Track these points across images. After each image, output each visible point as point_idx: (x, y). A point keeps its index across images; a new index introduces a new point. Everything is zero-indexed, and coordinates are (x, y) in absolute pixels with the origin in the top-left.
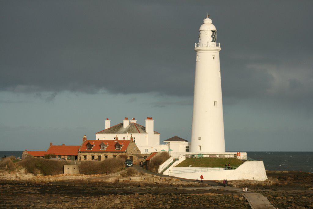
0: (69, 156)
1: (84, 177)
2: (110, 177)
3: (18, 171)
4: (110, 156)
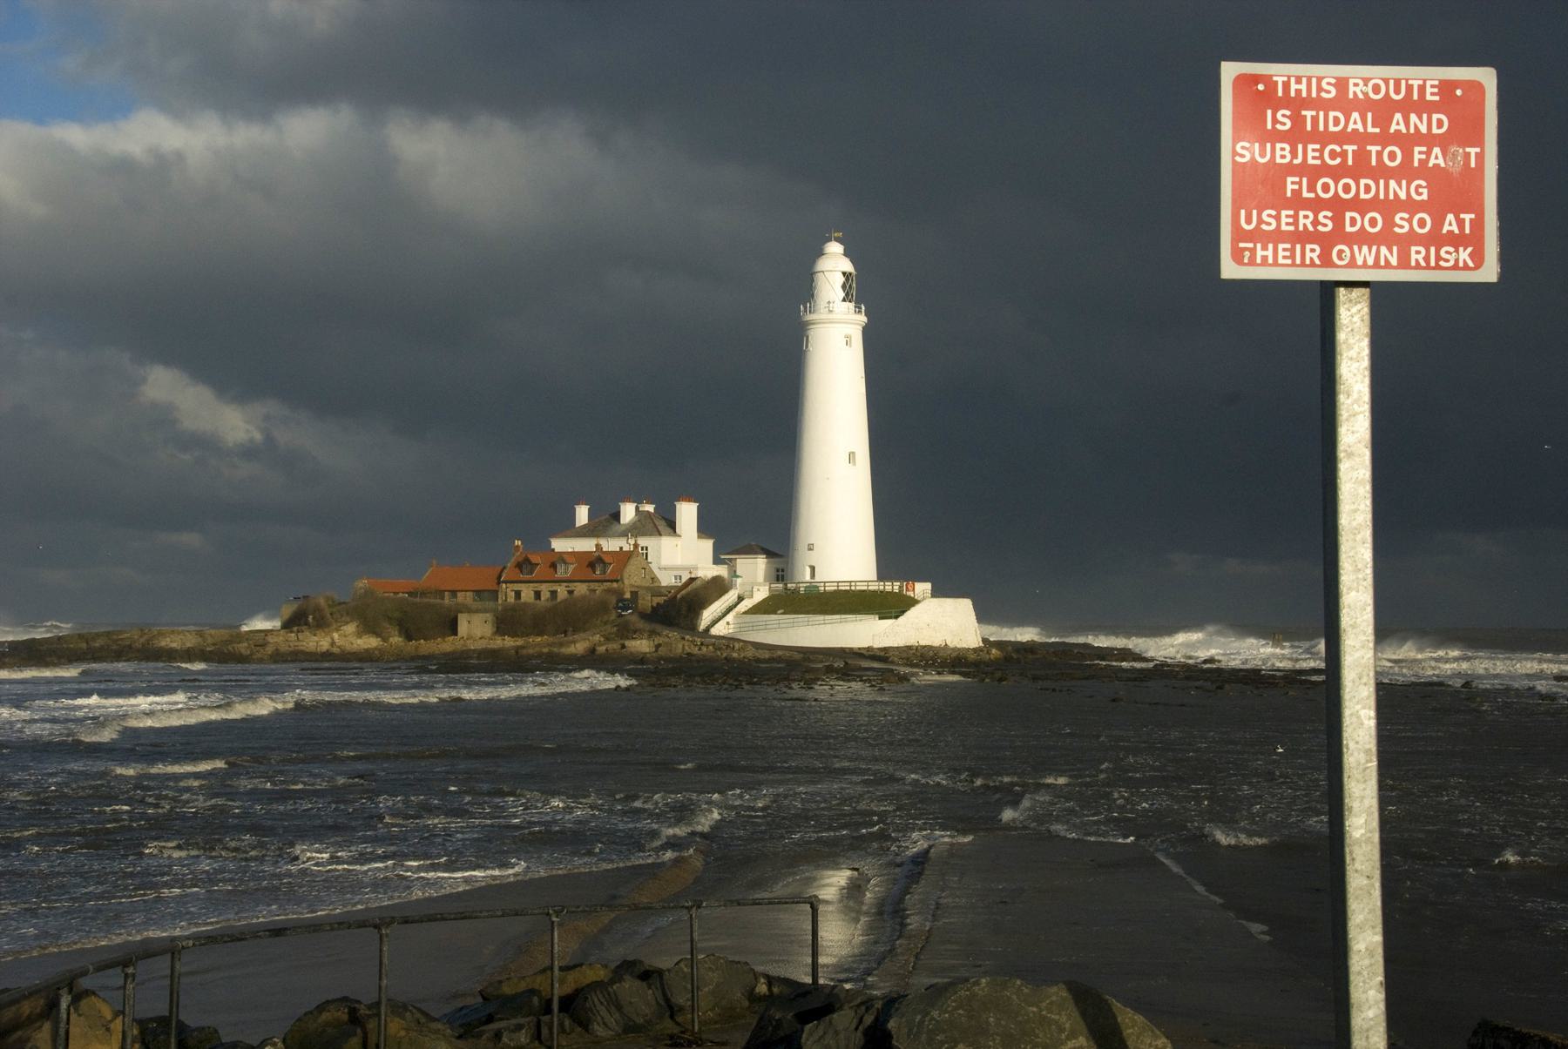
0: (478, 592)
1: (509, 642)
2: (574, 642)
3: (337, 630)
4: (581, 589)
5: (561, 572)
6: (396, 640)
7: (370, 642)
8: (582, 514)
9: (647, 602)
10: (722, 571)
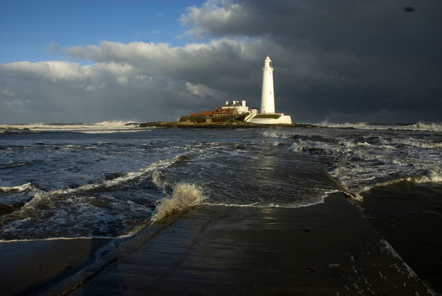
4: (226, 115)
5: (223, 112)
6: (196, 123)
7: (192, 123)
8: (227, 103)
9: (237, 117)
10: (250, 112)
